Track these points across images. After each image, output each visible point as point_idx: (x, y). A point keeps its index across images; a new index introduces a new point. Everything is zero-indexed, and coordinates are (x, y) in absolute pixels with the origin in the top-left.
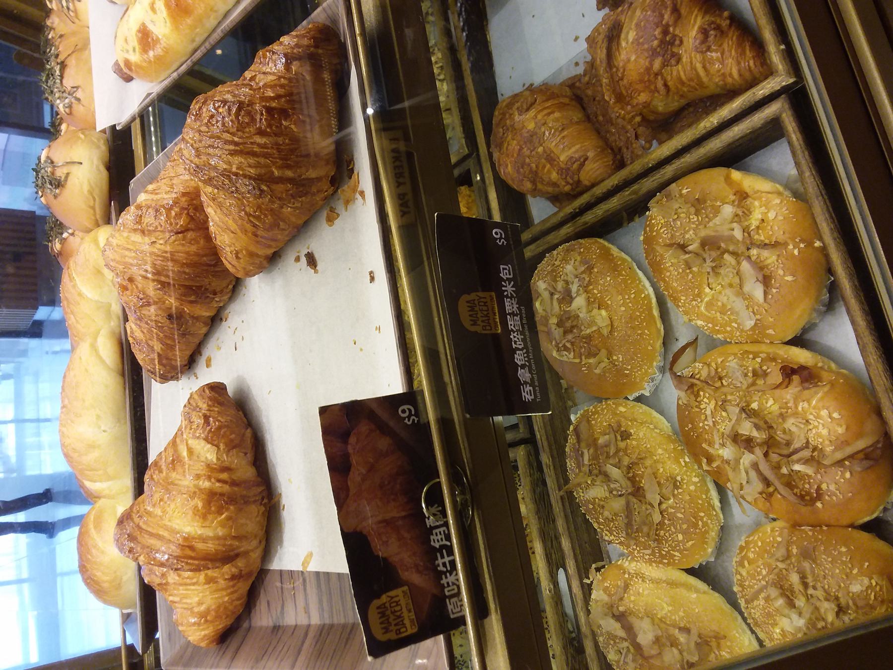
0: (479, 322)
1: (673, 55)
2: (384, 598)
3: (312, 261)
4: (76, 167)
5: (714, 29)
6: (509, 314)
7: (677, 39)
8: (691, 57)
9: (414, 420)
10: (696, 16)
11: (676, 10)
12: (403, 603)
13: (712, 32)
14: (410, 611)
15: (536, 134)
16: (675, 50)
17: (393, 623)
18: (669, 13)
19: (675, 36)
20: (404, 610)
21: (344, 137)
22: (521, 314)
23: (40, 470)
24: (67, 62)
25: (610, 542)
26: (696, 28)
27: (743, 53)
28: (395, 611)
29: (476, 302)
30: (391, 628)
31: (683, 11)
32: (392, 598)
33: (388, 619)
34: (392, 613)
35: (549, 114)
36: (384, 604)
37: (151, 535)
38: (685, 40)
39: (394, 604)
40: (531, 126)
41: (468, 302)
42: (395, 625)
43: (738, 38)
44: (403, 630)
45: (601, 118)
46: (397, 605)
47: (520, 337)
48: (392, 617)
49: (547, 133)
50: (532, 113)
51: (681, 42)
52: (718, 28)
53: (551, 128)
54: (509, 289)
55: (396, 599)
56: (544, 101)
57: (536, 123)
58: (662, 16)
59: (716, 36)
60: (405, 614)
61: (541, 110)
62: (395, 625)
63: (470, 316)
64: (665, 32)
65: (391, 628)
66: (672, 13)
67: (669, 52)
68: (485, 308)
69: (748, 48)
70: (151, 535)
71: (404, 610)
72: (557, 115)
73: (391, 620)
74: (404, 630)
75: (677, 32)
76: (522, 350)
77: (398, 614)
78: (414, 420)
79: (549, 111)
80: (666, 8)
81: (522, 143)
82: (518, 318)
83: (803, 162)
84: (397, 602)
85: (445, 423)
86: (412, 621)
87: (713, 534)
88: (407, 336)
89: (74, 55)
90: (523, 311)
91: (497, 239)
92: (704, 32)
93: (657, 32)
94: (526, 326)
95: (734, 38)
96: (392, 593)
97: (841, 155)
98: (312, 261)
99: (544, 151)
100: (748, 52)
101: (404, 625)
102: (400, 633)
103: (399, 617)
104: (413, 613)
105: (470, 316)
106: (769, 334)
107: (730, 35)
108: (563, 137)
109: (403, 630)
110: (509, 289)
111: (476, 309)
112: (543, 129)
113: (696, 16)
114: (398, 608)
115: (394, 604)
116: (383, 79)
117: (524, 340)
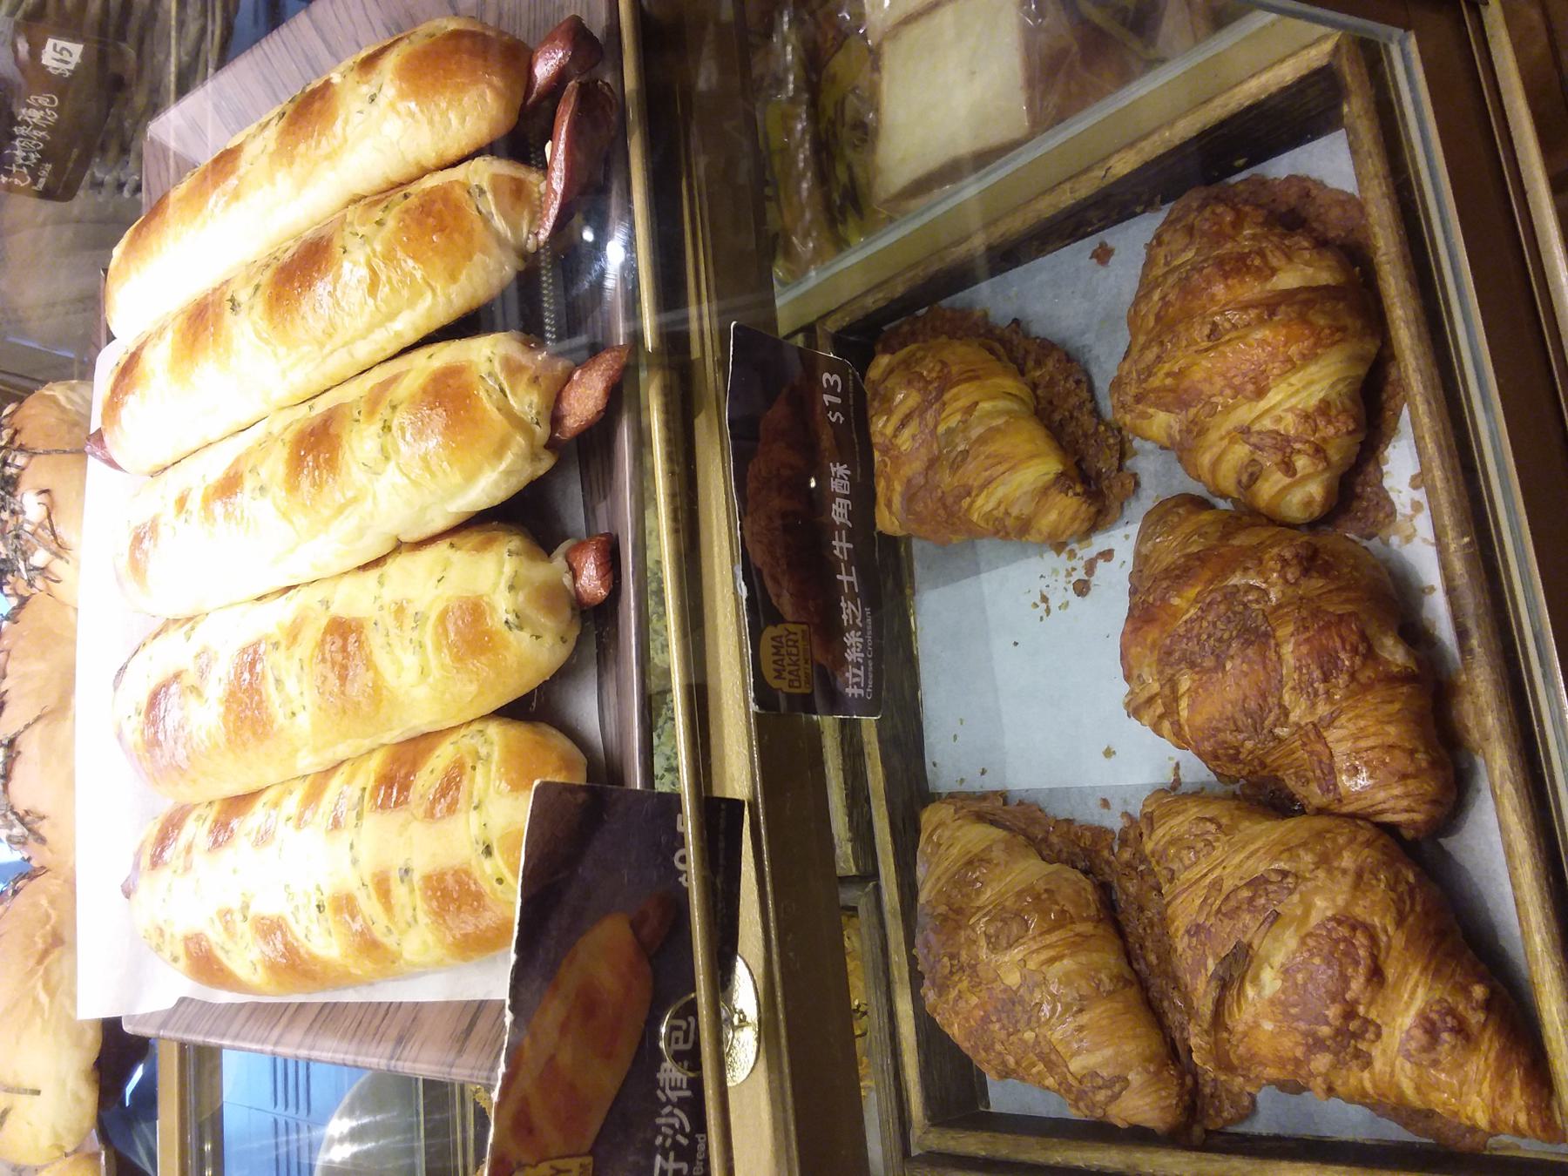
0: (785, 674)
1: (1358, 1054)
4: (23, 1101)
5: (1451, 1030)
7: (1372, 1029)
8: (1393, 1066)
10: (1416, 986)
11: (1376, 975)
13: (1445, 1036)
15: (1022, 1001)
16: (1363, 1046)
18: (1362, 979)
19: (1367, 1022)
24: (23, 744)
26: (1413, 1011)
27: (1506, 1095)
31: (1391, 973)
35: (1052, 961)
38: (1385, 1030)
40: (1013, 979)
43: (1499, 1058)
45: (1153, 958)
49: (1046, 1008)
50: (1017, 953)
51: (1378, 1035)
52: (1461, 1030)
53: (1055, 998)
56: (1041, 934)
57: (1023, 977)
58: (1345, 980)
59: (1454, 1047)
61: (1037, 951)
64: (1350, 1014)
66: (1369, 981)
67: (1350, 1050)
68: (794, 651)
69: (1517, 1082)
72: (1067, 964)
75: (1373, 1015)
79: (1052, 953)
80: (1357, 963)
81: (990, 1008)
83: (1426, 420)
85: (699, 302)
89: (38, 727)
92: (1430, 1029)
93: (1333, 1012)
95: (1492, 1055)
97: (1538, 638)
99: (1037, 1042)
100: (1516, 1092)
107: (1484, 1047)
108: (1080, 1029)
112: (1037, 996)
113: (1416, 986)
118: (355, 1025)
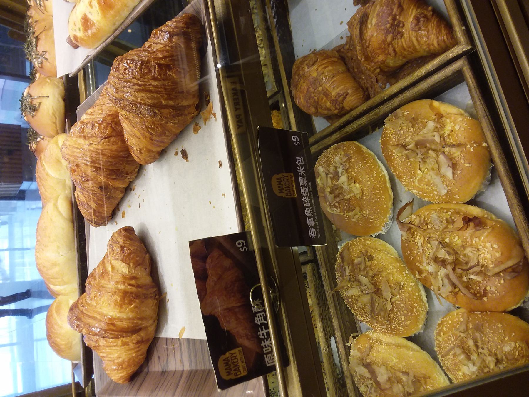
0: (284, 191)
1: (399, 33)
2: (227, 355)
3: (185, 155)
4: (45, 99)
5: (423, 17)
6: (302, 186)
7: (401, 23)
8: (409, 34)
9: (245, 249)
10: (413, 10)
11: (400, 6)
12: (239, 357)
13: (422, 19)
14: (243, 362)
15: (317, 79)
16: (400, 30)
17: (233, 369)
18: (396, 8)
19: (400, 21)
20: (240, 361)
21: (204, 81)
22: (308, 186)
23: (24, 278)
24: (40, 37)
25: (361, 321)
26: (412, 17)
27: (440, 31)
28: (234, 362)
29: (282, 179)
30: (232, 372)
31: (405, 7)
32: (232, 354)
33: (230, 367)
34: (232, 363)
35: (325, 68)
36: (228, 358)
37: (90, 317)
38: (406, 23)
39: (234, 358)
40: (315, 75)
41: (277, 179)
42: (234, 370)
43: (437, 23)
44: (238, 373)
45: (356, 70)
46: (235, 358)
47: (308, 200)
48: (232, 366)
49: (324, 79)
50: (315, 67)
51: (404, 25)
52: (425, 17)
53: (326, 76)
54: (302, 171)
55: (235, 355)
56: (322, 60)
57: (317, 73)
58: (392, 9)
59: (424, 21)
60: (240, 364)
61: (321, 65)
62: (234, 370)
63: (279, 187)
64: (394, 19)
65: (232, 372)
66: (398, 8)
67: (396, 31)
68: (287, 183)
69: (443, 28)
70: (90, 317)
71: (240, 361)
72: (330, 68)
73: (231, 367)
74: (239, 373)
75: (401, 19)
76: (309, 207)
77: (236, 364)
78: (245, 249)
79: (325, 66)
80: (395, 5)
81: (309, 85)
82: (307, 189)
84: (235, 357)
86: (244, 368)
87: (423, 317)
88: (241, 199)
89: (44, 33)
90: (310, 184)
91: (294, 142)
92: (417, 19)
93: (389, 19)
94: (312, 193)
95: (435, 22)
96: (232, 352)
98: (185, 155)
99: (323, 90)
100: (443, 31)
101: (239, 370)
102: (237, 375)
103: (237, 365)
104: (244, 363)
106: (456, 198)
107: (432, 21)
108: (334, 81)
109: (238, 373)
110: (302, 171)
111: (282, 183)
112: (322, 77)
113: (413, 10)
114: (236, 360)
115: (234, 358)
116: (227, 47)
117: (310, 202)
118: (169, 384)
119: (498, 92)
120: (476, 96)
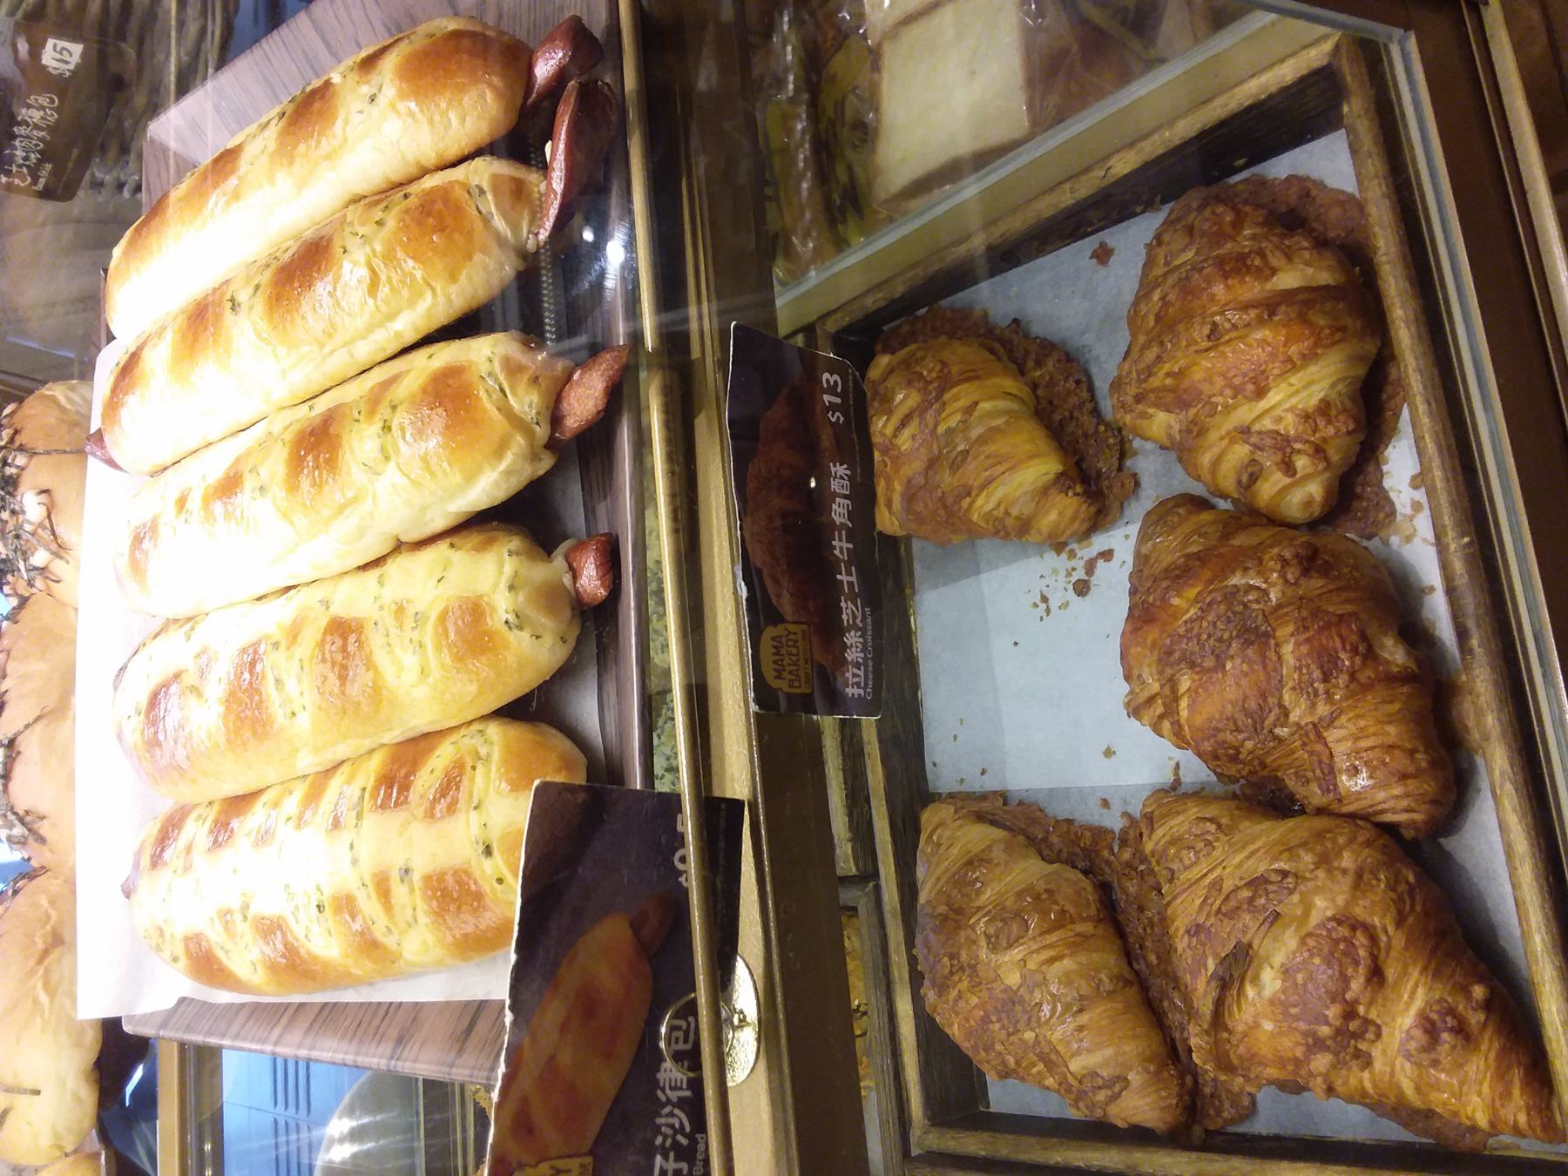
0: (785, 674)
1: (1358, 1054)
4: (23, 1101)
5: (1451, 1030)
7: (1372, 1029)
8: (1393, 1066)
10: (1416, 986)
11: (1376, 975)
13: (1445, 1036)
15: (1022, 1001)
16: (1363, 1046)
18: (1362, 979)
19: (1367, 1022)
24: (23, 744)
26: (1413, 1011)
27: (1506, 1095)
31: (1391, 973)
35: (1052, 961)
38: (1385, 1030)
40: (1013, 979)
43: (1499, 1058)
45: (1153, 958)
49: (1046, 1008)
50: (1017, 953)
51: (1378, 1035)
52: (1461, 1030)
53: (1055, 998)
56: (1041, 934)
57: (1023, 977)
58: (1345, 980)
59: (1454, 1047)
61: (1037, 951)
64: (1350, 1014)
66: (1369, 981)
67: (1350, 1050)
68: (794, 651)
69: (1517, 1082)
72: (1067, 964)
75: (1373, 1015)
79: (1052, 953)
80: (1357, 963)
81: (990, 1008)
89: (38, 727)
92: (1430, 1029)
93: (1333, 1012)
95: (1492, 1055)
99: (1037, 1042)
100: (1516, 1092)
105: (775, 662)
107: (1484, 1047)
108: (1080, 1029)
112: (1037, 996)
113: (1416, 986)
118: (355, 1025)
119: (1538, 638)
120: (1426, 420)
